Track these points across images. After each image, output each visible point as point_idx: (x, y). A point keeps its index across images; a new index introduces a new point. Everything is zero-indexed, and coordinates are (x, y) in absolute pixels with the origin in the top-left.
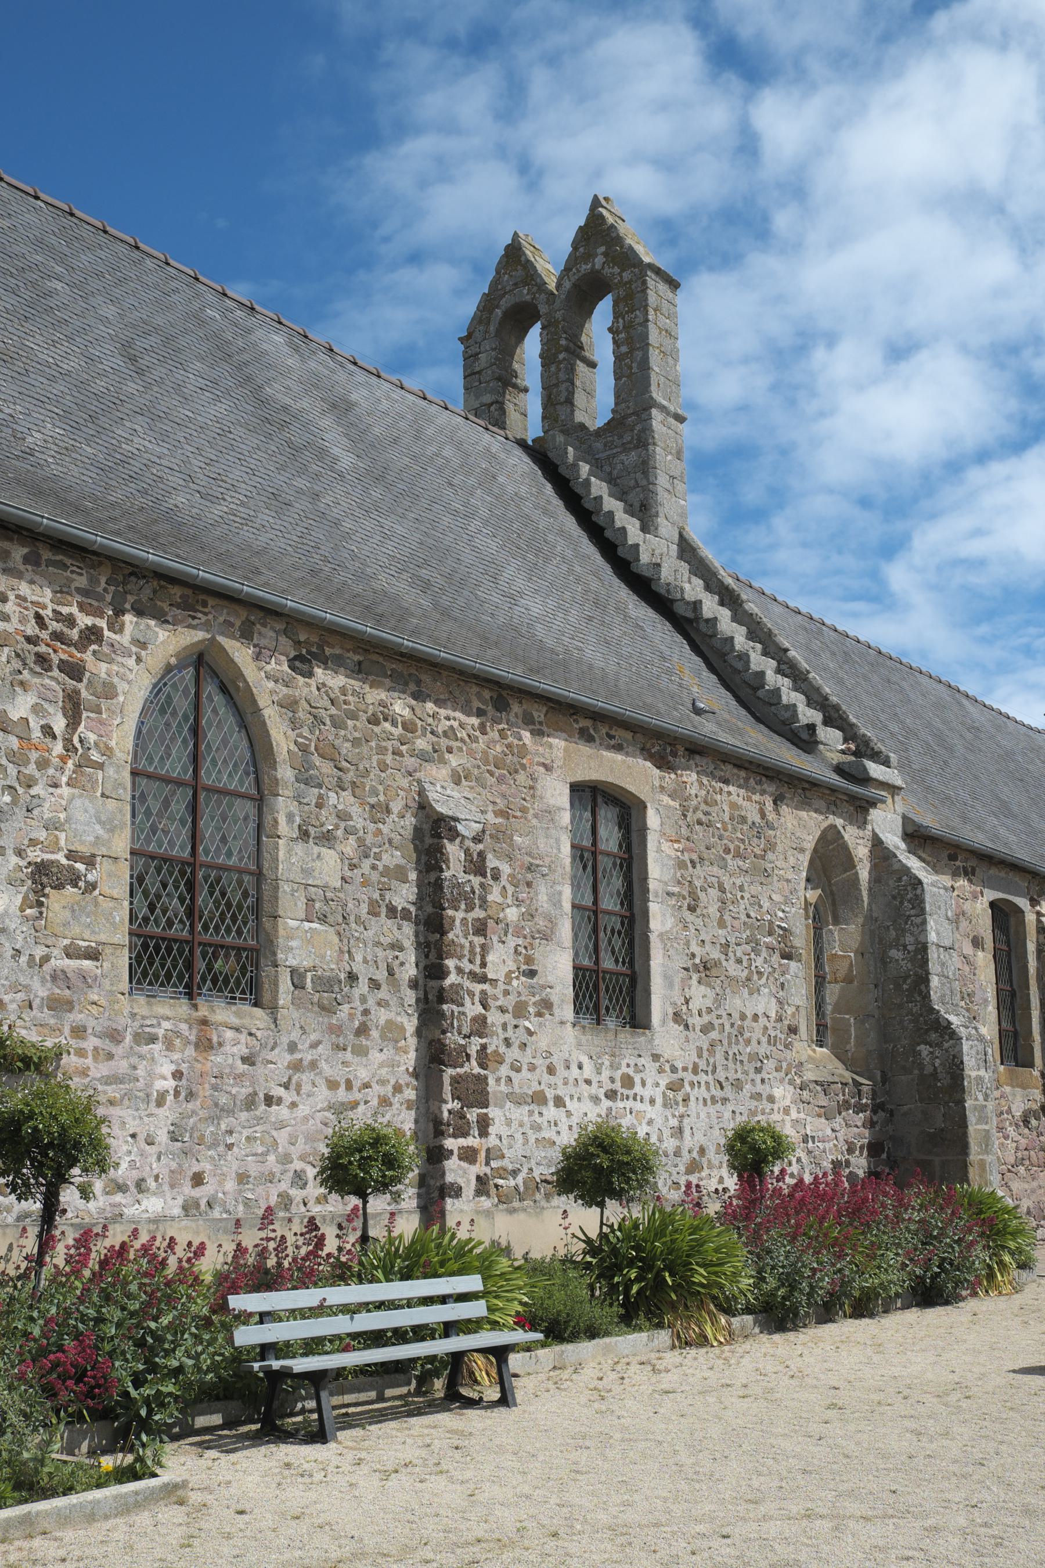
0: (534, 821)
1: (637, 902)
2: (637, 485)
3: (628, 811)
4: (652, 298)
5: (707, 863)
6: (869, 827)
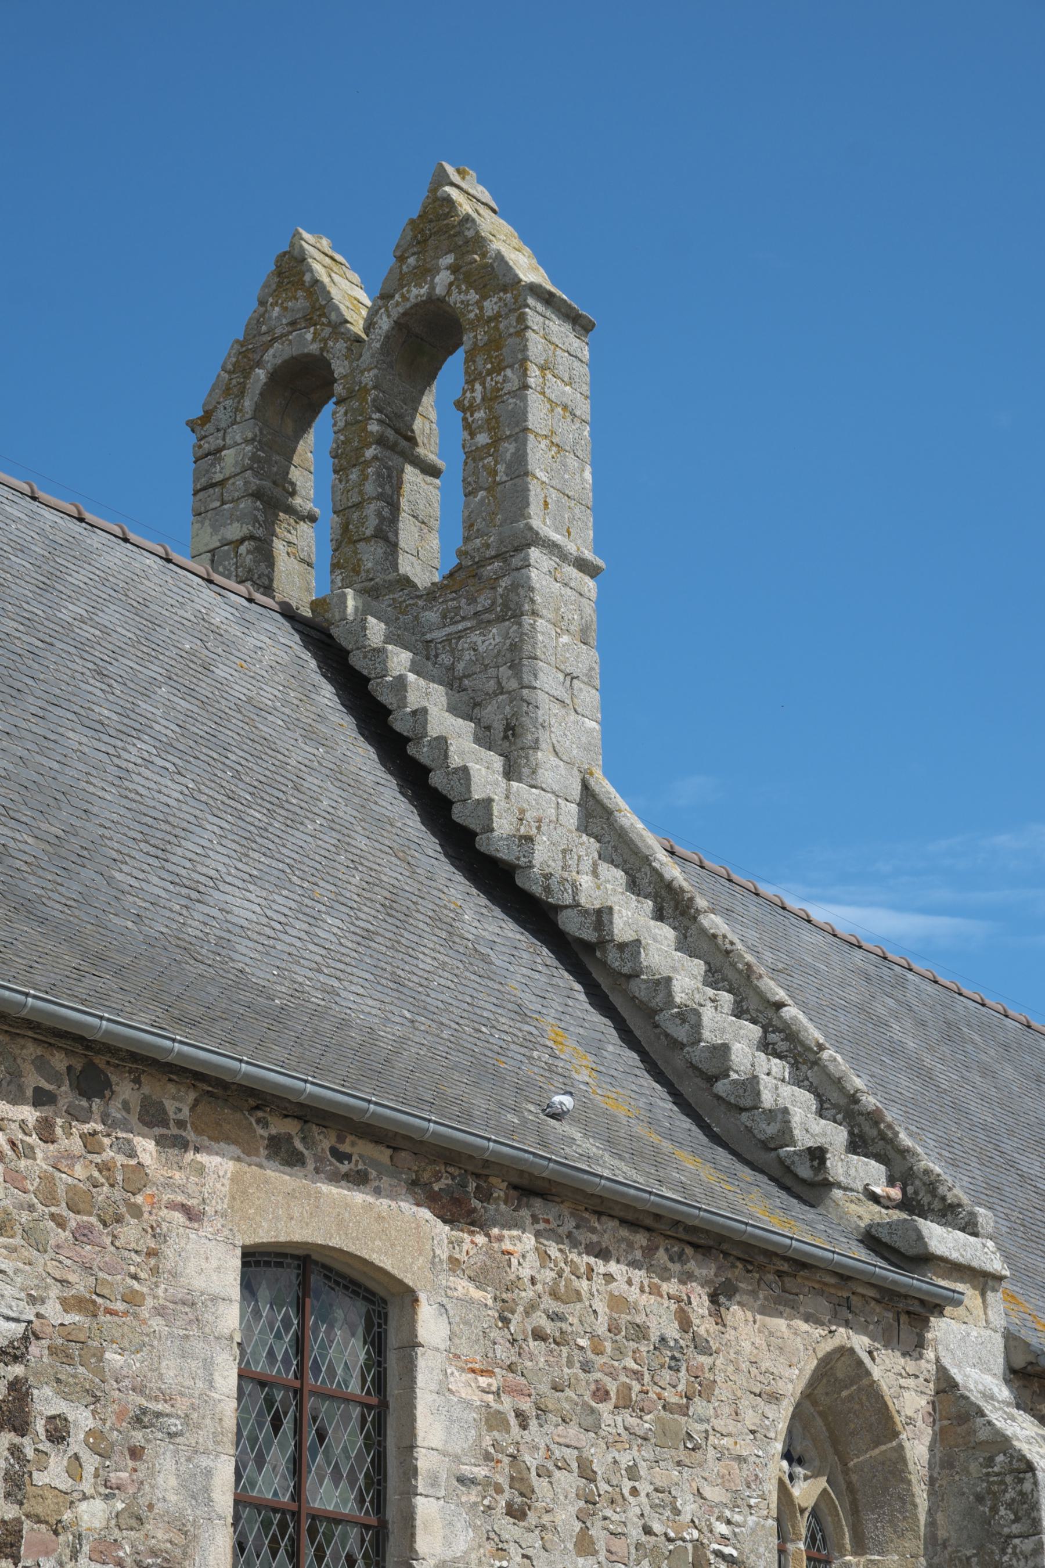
0: (156, 1323)
1: (393, 1496)
2: (501, 690)
3: (379, 1304)
4: (536, 346)
5: (553, 1418)
6: (929, 1354)
